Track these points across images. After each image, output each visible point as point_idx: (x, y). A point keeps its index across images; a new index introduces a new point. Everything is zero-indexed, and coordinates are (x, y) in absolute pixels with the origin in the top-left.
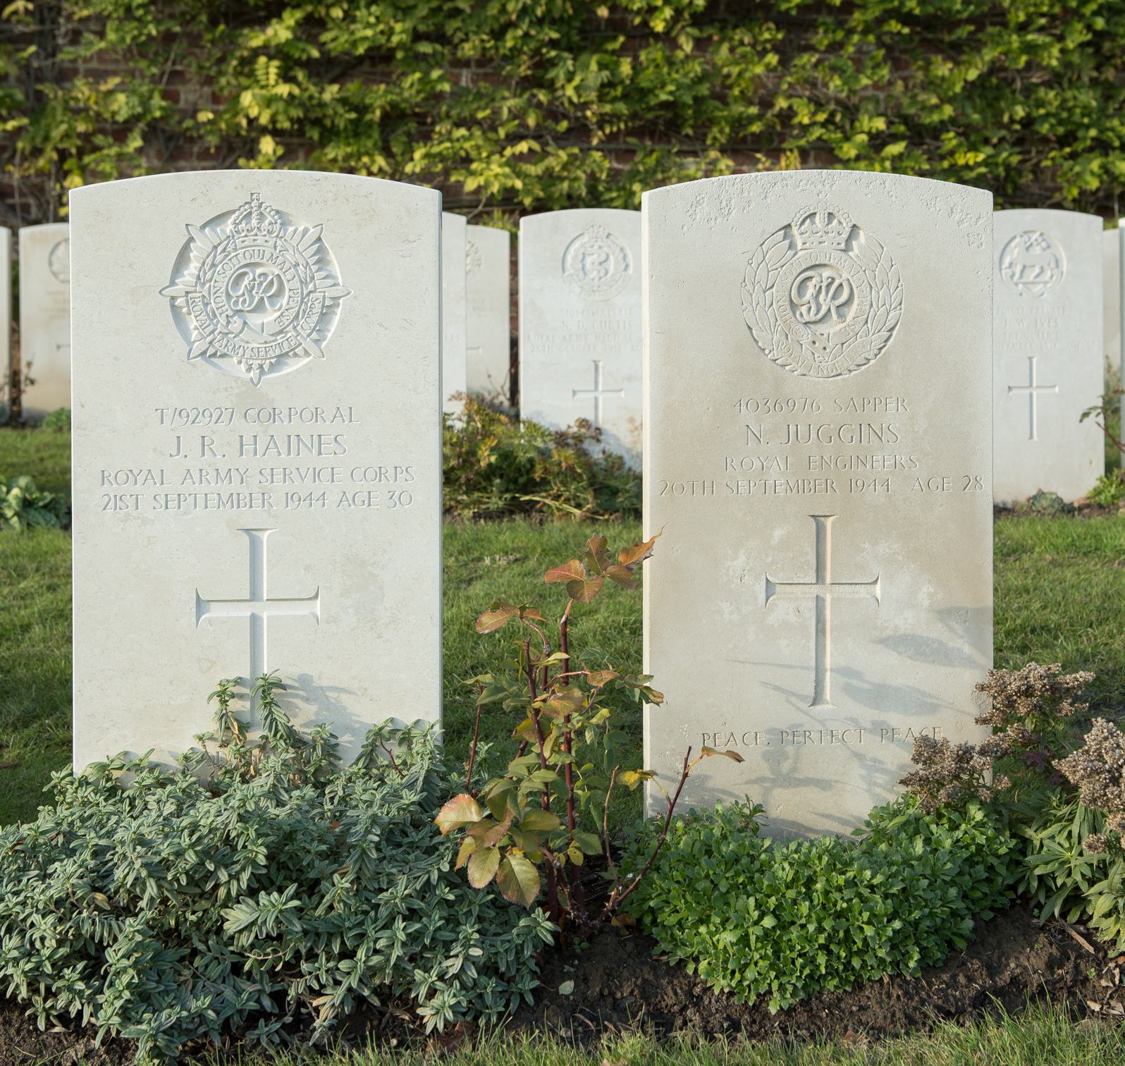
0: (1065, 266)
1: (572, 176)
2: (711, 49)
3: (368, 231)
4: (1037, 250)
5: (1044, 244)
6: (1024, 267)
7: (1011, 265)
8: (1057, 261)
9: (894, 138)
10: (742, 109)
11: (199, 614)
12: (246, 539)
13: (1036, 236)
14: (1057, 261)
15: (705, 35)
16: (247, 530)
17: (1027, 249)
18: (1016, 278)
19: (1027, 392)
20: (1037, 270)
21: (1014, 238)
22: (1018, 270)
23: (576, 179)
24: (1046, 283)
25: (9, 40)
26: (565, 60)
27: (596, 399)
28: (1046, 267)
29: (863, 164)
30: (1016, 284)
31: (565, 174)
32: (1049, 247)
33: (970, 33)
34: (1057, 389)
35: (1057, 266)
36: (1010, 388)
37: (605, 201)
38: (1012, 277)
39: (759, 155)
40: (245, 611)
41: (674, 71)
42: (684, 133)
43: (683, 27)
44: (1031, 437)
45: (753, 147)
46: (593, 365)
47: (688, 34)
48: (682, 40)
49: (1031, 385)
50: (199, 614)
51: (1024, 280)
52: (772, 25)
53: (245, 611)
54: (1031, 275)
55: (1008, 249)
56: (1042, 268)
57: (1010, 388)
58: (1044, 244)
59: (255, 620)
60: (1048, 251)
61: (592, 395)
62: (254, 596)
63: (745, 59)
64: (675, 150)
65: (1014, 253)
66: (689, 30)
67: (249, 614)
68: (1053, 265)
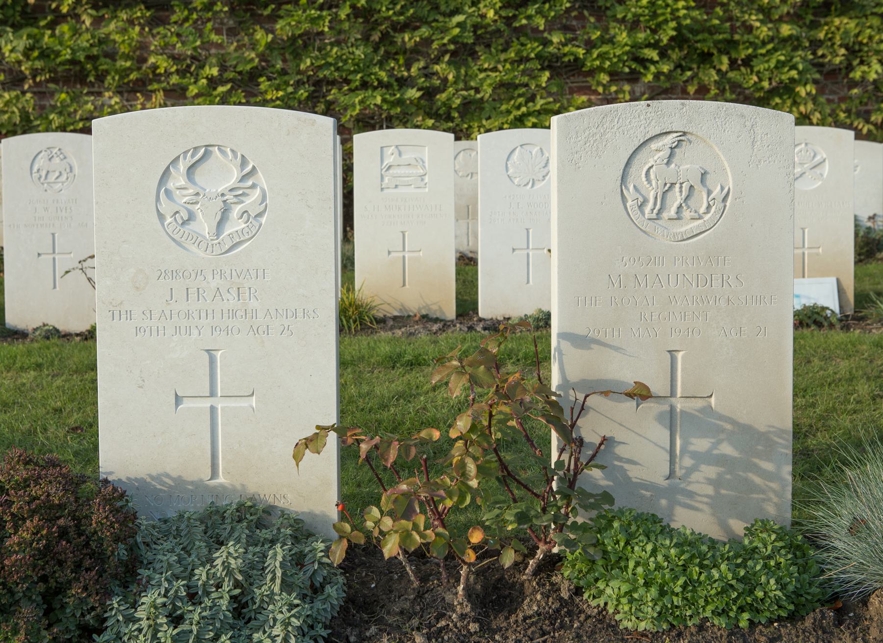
0: (76, 170)
1: (10, 110)
2: (103, 24)
3: (288, 142)
4: (57, 160)
5: (61, 156)
6: (48, 172)
7: (38, 170)
8: (71, 168)
9: (223, 82)
10: (123, 63)
11: (177, 404)
12: (206, 355)
13: (55, 151)
14: (71, 168)
15: (100, 14)
16: (207, 351)
17: (50, 159)
18: (42, 180)
19: (525, 252)
20: (57, 174)
21: (41, 152)
22: (43, 174)
23: (13, 112)
24: (63, 183)
25: (637, 2)
26: (7, 32)
27: (528, 255)
28: (63, 172)
29: (200, 100)
30: (43, 184)
31: (6, 109)
32: (65, 158)
33: (273, 10)
34: (820, 250)
35: (71, 171)
36: (39, 255)
37: (34, 126)
38: (39, 178)
39: (138, 95)
40: (207, 404)
41: (69, 41)
42: (88, 80)
43: (86, 9)
44: (528, 282)
45: (137, 90)
46: (51, 237)
47: (88, 14)
48: (84, 17)
49: (528, 248)
50: (177, 404)
51: (48, 180)
52: (143, 7)
53: (207, 404)
54: (52, 177)
55: (645, 151)
56: (60, 173)
57: (39, 255)
58: (61, 156)
59: (213, 409)
60: (65, 161)
61: (525, 252)
62: (213, 394)
63: (121, 30)
64: (85, 91)
65: (40, 162)
66: (89, 11)
67: (209, 405)
68: (68, 170)
